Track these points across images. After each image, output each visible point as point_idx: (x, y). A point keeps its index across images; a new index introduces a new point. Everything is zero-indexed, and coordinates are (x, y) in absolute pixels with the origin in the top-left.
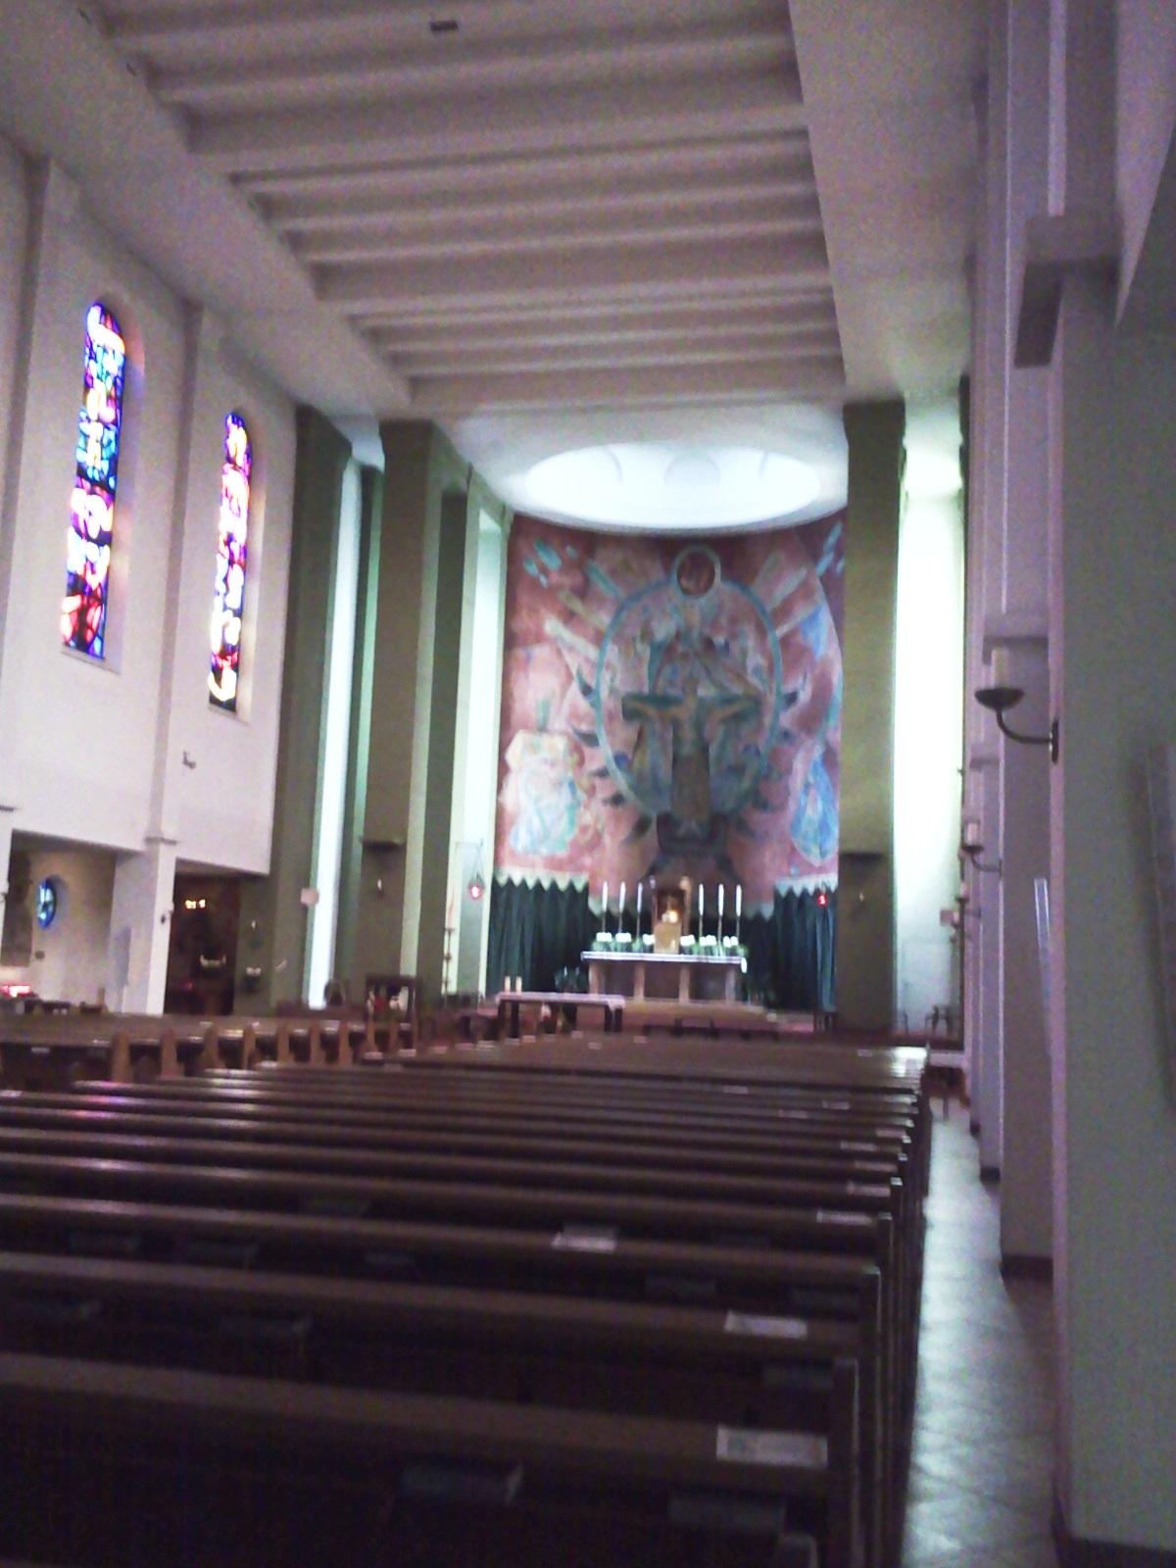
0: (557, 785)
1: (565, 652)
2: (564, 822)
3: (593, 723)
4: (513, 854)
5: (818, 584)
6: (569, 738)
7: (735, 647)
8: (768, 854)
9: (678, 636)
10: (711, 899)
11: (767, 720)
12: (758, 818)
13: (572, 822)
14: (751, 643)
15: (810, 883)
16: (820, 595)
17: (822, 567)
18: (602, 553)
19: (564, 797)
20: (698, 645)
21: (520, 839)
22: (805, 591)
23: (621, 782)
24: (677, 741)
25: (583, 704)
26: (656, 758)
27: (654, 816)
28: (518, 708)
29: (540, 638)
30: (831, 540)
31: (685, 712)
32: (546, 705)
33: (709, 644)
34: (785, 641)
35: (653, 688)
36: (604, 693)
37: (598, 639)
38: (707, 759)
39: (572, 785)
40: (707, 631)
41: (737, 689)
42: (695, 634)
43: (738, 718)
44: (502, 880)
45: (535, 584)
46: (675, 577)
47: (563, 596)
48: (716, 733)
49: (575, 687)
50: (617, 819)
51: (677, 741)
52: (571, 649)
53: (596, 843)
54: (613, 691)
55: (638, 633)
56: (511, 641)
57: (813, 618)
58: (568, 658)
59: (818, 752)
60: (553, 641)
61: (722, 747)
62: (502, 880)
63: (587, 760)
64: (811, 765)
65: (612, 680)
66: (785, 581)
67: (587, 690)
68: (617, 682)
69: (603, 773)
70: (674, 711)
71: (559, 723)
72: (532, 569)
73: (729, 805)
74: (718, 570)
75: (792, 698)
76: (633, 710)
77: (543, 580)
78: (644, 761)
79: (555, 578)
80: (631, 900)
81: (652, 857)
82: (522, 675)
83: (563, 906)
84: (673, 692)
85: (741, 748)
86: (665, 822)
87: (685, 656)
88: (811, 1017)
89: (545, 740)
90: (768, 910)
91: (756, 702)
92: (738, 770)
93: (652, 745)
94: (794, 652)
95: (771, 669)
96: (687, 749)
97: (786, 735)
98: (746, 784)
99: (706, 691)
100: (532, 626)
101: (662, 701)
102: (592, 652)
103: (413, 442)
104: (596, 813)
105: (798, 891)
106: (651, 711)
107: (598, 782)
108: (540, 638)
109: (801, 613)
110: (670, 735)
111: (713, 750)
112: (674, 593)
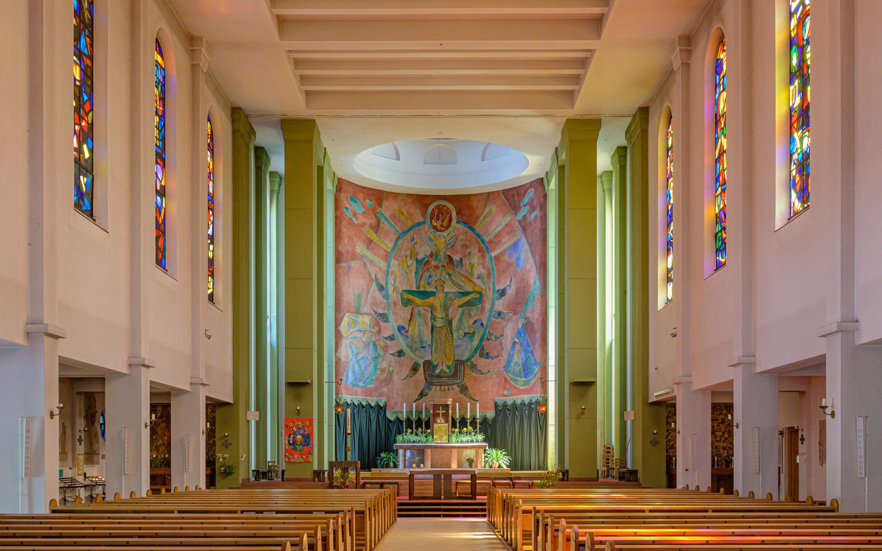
1: (368, 265)
5: (517, 224)
6: (373, 317)
9: (431, 255)
10: (463, 408)
11: (488, 306)
12: (482, 363)
13: (376, 367)
14: (475, 260)
16: (519, 233)
17: (520, 216)
19: (369, 354)
20: (444, 262)
21: (349, 378)
24: (433, 318)
25: (379, 296)
27: (421, 362)
29: (355, 256)
30: (526, 200)
33: (450, 260)
34: (497, 258)
36: (390, 291)
37: (386, 257)
38: (451, 330)
39: (375, 345)
40: (448, 253)
42: (442, 254)
45: (351, 223)
48: (456, 314)
49: (374, 285)
51: (433, 318)
52: (371, 262)
53: (389, 380)
54: (395, 289)
55: (408, 253)
57: (515, 246)
58: (370, 268)
60: (361, 257)
61: (460, 321)
67: (381, 288)
68: (397, 284)
69: (392, 338)
71: (366, 309)
72: (349, 214)
75: (503, 293)
77: (354, 219)
78: (414, 330)
79: (362, 219)
80: (419, 412)
84: (431, 289)
85: (472, 321)
87: (437, 267)
88: (555, 471)
89: (360, 318)
90: (491, 414)
92: (470, 335)
93: (418, 320)
95: (489, 275)
96: (439, 323)
97: (499, 314)
98: (475, 343)
99: (449, 288)
101: (425, 295)
102: (383, 264)
103: (299, 132)
104: (388, 362)
105: (519, 402)
106: (418, 301)
107: (389, 342)
108: (355, 256)
109: (507, 242)
110: (429, 315)
111: (455, 323)
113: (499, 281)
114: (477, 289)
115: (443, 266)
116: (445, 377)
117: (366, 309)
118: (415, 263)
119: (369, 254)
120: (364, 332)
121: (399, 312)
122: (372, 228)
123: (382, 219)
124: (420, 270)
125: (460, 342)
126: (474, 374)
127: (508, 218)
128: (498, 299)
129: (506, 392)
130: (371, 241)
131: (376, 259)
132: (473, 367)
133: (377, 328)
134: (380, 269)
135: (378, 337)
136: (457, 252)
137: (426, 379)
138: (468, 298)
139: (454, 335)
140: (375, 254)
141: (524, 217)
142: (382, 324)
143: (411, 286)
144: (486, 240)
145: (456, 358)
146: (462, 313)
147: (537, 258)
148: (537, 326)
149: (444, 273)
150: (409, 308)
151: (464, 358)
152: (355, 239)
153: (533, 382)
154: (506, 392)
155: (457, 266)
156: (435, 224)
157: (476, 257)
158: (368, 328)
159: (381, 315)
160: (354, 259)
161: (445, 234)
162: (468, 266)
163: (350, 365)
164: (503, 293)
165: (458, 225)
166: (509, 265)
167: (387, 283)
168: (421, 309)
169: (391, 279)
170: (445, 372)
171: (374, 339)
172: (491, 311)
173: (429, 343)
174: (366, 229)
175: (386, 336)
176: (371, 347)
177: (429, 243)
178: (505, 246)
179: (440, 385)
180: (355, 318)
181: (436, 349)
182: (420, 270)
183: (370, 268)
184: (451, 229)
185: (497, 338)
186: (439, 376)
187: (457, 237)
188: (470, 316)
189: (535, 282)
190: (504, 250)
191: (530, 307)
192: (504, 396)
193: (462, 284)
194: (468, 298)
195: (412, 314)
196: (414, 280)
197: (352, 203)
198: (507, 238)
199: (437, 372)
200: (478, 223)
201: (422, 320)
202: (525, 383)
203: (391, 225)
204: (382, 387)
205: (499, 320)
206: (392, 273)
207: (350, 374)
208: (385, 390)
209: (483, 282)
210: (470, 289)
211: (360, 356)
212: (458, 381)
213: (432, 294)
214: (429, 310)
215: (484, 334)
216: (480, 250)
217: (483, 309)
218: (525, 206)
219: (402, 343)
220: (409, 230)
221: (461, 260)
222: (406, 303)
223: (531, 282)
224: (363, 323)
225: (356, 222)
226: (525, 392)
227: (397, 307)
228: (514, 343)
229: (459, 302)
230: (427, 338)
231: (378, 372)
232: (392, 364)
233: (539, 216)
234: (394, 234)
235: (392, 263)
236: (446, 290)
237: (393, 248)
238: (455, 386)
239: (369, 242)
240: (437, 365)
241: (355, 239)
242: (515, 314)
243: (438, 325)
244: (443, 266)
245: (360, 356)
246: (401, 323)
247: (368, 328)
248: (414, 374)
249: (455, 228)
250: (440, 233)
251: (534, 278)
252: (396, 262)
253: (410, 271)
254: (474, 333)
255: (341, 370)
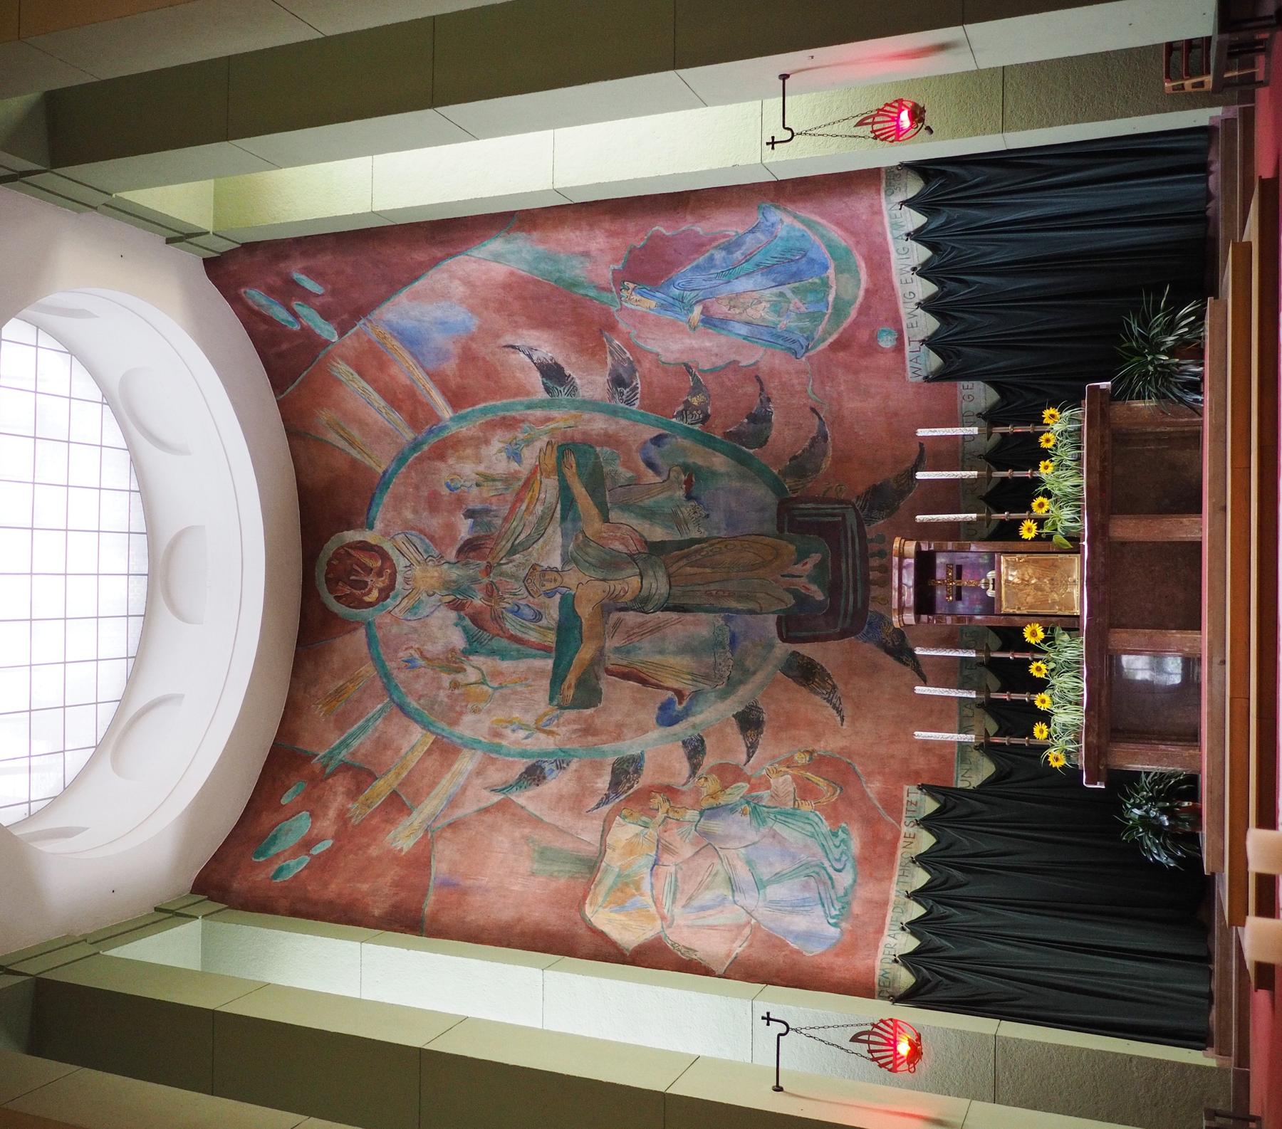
0: (707, 843)
1: (458, 813)
2: (791, 834)
3: (596, 767)
4: (846, 948)
6: (617, 811)
7: (474, 498)
8: (852, 404)
9: (456, 606)
10: (948, 496)
11: (599, 424)
12: (786, 434)
13: (788, 816)
15: (907, 257)
17: (326, 331)
18: (306, 743)
19: (738, 832)
21: (812, 929)
22: (371, 363)
23: (714, 714)
24: (641, 604)
25: (557, 783)
26: (672, 646)
27: (782, 649)
28: (542, 914)
29: (420, 861)
31: (588, 589)
32: (545, 854)
33: (470, 548)
34: (457, 399)
35: (545, 649)
36: (544, 743)
37: (446, 750)
38: (680, 545)
39: (713, 812)
40: (452, 554)
41: (549, 488)
42: (455, 573)
43: (596, 482)
44: (905, 979)
45: (324, 865)
46: (366, 613)
47: (357, 810)
49: (522, 798)
50: (789, 723)
51: (641, 604)
52: (453, 803)
53: (838, 770)
54: (541, 727)
55: (446, 679)
56: (407, 921)
57: (412, 342)
58: (467, 809)
59: (639, 302)
61: (649, 514)
62: (905, 979)
63: (666, 780)
64: (668, 316)
65: (522, 726)
66: (363, 415)
67: (534, 775)
69: (695, 750)
70: (585, 611)
71: (588, 833)
73: (761, 493)
74: (352, 536)
75: (553, 374)
76: (578, 689)
78: (677, 669)
79: (328, 824)
81: (868, 650)
82: (476, 900)
83: (967, 844)
84: (553, 613)
85: (650, 477)
86: (793, 626)
87: (491, 591)
89: (613, 861)
90: (979, 394)
91: (570, 449)
92: (693, 479)
93: (645, 654)
94: (471, 380)
95: (509, 423)
97: (618, 382)
98: (719, 462)
100: (393, 874)
101: (568, 628)
102: (466, 763)
104: (774, 766)
106: (586, 653)
107: (709, 761)
108: (420, 861)
109: (407, 370)
110: (631, 618)
111: (658, 533)
112: (389, 617)
113: (520, 390)
114: (551, 462)
115: (488, 570)
116: (837, 569)
117: (588, 833)
118: (477, 660)
119: (430, 806)
120: (663, 848)
121: (618, 717)
122: (354, 794)
123: (344, 755)
124: (495, 644)
125: (717, 517)
126: (826, 464)
127: (342, 370)
128: (574, 389)
129: (887, 342)
130: (394, 795)
131: (447, 785)
132: (801, 466)
133: (658, 800)
134: (479, 773)
135: (687, 800)
136: (450, 527)
137: (843, 635)
138: (579, 490)
139: (695, 534)
140: (433, 785)
141: (326, 314)
142: (645, 780)
143: (539, 673)
144: (409, 435)
145: (771, 527)
146: (625, 507)
147: (420, 256)
148: (639, 233)
149: (508, 568)
150: (607, 684)
151: (770, 499)
152: (374, 851)
153: (836, 234)
154: (887, 342)
155: (489, 524)
156: (375, 594)
157: (458, 467)
158: (652, 833)
159: (615, 785)
160: (428, 865)
161: (401, 563)
162: (488, 492)
163: (764, 915)
164: (553, 374)
165: (378, 525)
166: (468, 357)
167: (523, 754)
168: (610, 644)
169: (514, 738)
170: (820, 566)
171: (692, 815)
172: (614, 412)
173: (718, 620)
174: (357, 810)
175: (685, 768)
176: (717, 826)
177: (424, 611)
178: (419, 374)
179: (867, 583)
180: (609, 881)
181: (740, 597)
182: (495, 644)
183: (467, 809)
184: (388, 547)
185: (697, 388)
186: (834, 589)
187: (407, 527)
188: (634, 482)
189: (497, 258)
190: (431, 375)
191: (577, 270)
192: (899, 347)
193: (539, 509)
194: (579, 490)
195: (625, 676)
196: (523, 665)
197: (274, 850)
198: (394, 370)
199: (819, 596)
200: (368, 462)
201: (646, 644)
202: (844, 267)
203: (363, 729)
204: (864, 795)
205: (638, 381)
206: (497, 734)
207: (800, 923)
208: (873, 788)
209: (529, 442)
210: (549, 487)
211: (743, 873)
212: (851, 520)
213: (568, 605)
214: (615, 616)
215: (689, 433)
216: (440, 453)
217: (610, 440)
218: (295, 315)
219: (714, 714)
220: (386, 675)
221: (470, 514)
222: (588, 695)
223: (499, 272)
224: (631, 849)
225: (328, 844)
226: (878, 262)
227: (598, 722)
228: (709, 321)
229: (593, 525)
230: (702, 626)
231: (806, 807)
232: (784, 753)
233: (301, 264)
234: (388, 719)
235: (468, 733)
236: (556, 561)
237: (426, 726)
238: (871, 531)
239: (397, 805)
240: (795, 593)
241: (374, 851)
242: (611, 327)
243: (664, 589)
244: (488, 570)
245: (743, 873)
246: (649, 715)
247: (652, 833)
248: (824, 675)
249: (385, 534)
250: (399, 579)
251: (495, 260)
252: (468, 718)
253: (497, 674)
254: (686, 468)
255: (779, 959)
